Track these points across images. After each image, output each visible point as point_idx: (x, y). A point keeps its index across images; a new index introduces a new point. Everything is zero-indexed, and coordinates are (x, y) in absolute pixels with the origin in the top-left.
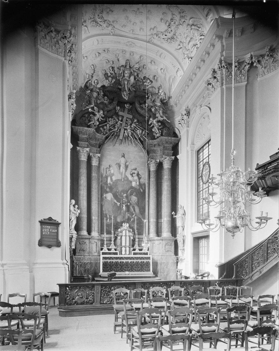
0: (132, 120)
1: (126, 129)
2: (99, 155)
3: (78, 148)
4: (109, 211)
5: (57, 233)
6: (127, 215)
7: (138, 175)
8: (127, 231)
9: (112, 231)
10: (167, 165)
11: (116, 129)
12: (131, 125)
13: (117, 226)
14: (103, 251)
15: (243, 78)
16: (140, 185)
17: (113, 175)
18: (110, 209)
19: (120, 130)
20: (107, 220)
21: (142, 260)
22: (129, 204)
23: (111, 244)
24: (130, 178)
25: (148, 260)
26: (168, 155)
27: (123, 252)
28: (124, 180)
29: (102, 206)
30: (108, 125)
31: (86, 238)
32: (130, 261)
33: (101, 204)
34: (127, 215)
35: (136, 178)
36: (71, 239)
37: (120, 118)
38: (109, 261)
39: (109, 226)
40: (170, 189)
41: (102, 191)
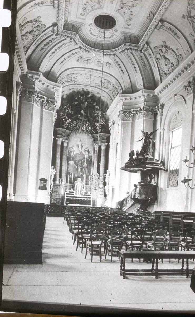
0: (86, 122)
1: (83, 127)
2: (67, 141)
3: (57, 138)
4: (71, 171)
5: (46, 184)
6: (81, 173)
7: (88, 151)
8: (80, 183)
9: (72, 182)
10: (103, 148)
11: (78, 127)
12: (85, 125)
13: (75, 179)
14: (67, 193)
15: (131, 119)
16: (89, 157)
17: (75, 151)
18: (72, 170)
19: (80, 127)
20: (70, 175)
21: (87, 199)
22: (82, 167)
23: (71, 189)
24: (84, 153)
25: (90, 199)
26: (104, 143)
27: (77, 194)
28: (80, 154)
29: (68, 168)
30: (73, 124)
31: (58, 186)
32: (80, 199)
33: (67, 167)
34: (81, 173)
35: (87, 153)
36: (51, 186)
37: (80, 121)
38: (69, 198)
39: (70, 179)
40: (104, 161)
41: (69, 160)
